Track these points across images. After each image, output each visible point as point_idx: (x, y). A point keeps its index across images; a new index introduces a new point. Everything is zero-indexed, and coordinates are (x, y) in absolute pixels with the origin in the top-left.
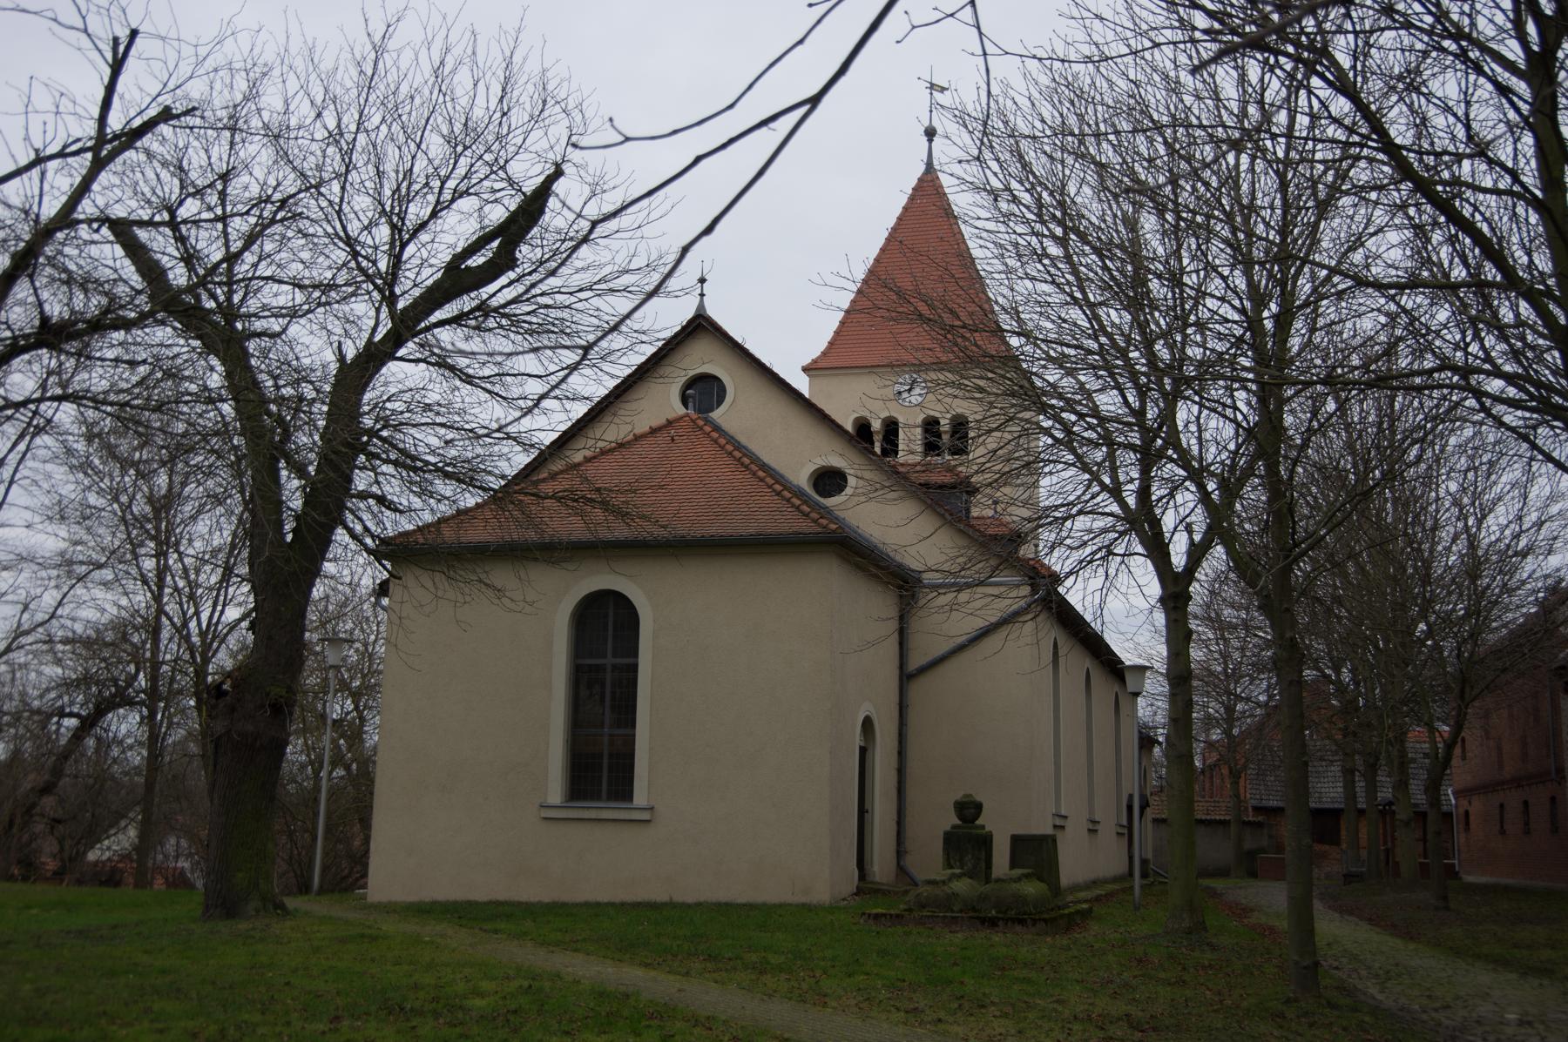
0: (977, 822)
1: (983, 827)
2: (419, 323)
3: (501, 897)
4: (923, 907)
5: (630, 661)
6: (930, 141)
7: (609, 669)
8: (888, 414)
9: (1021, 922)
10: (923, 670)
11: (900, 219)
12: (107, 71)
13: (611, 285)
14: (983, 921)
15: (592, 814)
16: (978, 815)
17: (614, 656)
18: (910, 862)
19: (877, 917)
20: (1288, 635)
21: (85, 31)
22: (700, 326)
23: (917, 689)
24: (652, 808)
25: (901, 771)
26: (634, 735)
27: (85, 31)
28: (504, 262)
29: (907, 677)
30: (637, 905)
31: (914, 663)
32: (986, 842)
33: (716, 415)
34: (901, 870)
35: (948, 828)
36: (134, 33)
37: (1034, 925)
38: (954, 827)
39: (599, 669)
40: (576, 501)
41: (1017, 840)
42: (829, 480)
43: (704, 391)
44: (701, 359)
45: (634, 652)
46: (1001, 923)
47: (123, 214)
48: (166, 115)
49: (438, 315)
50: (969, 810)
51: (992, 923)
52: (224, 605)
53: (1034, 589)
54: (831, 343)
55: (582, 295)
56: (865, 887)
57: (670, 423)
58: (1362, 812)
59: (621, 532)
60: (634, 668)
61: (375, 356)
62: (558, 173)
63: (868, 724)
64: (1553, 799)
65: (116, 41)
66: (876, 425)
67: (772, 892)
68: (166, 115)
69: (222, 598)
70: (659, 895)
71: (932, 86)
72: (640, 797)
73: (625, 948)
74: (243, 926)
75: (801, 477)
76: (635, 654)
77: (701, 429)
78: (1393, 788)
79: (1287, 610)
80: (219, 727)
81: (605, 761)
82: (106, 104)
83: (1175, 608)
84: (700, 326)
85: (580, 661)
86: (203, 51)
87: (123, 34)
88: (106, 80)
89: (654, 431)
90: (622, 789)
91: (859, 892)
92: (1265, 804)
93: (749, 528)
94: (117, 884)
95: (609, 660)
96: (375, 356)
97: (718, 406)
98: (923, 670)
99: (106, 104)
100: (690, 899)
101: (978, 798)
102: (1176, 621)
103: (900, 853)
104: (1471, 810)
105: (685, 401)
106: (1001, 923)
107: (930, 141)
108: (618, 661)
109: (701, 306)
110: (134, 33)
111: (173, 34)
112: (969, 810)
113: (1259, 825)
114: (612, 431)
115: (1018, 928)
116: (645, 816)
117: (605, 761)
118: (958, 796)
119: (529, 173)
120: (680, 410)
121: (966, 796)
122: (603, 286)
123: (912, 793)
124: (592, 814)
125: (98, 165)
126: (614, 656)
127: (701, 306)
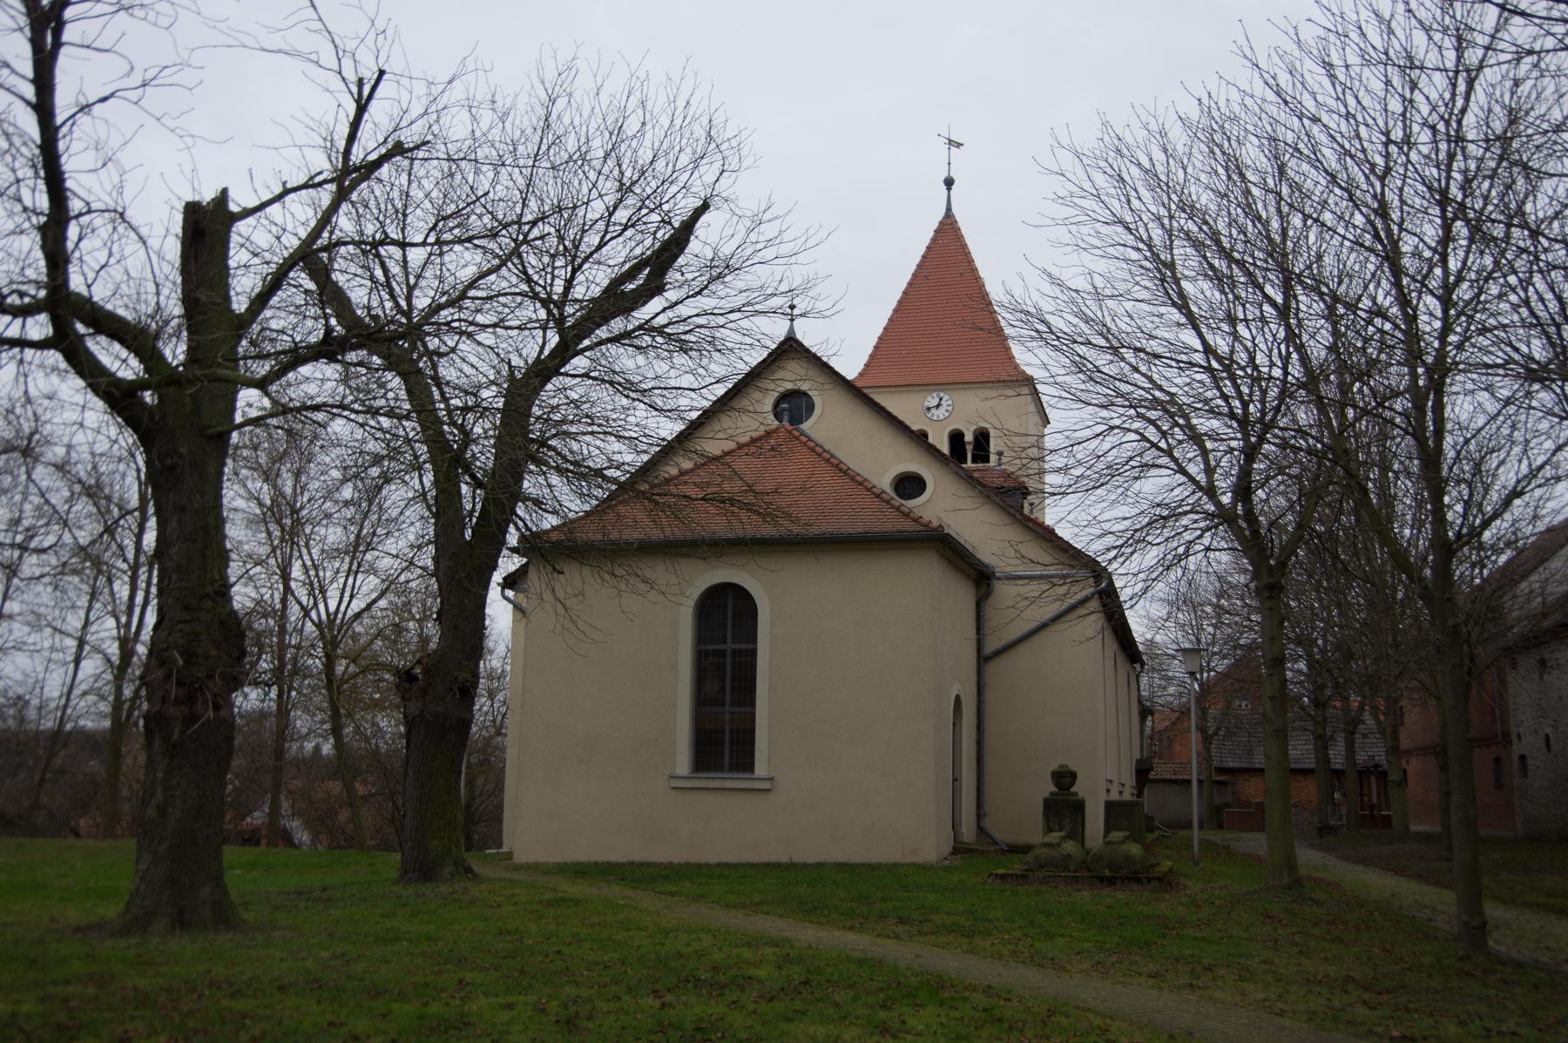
0: (1072, 790)
1: (1076, 794)
2: (581, 341)
3: (637, 858)
4: (1042, 867)
5: (749, 646)
6: (949, 189)
7: (729, 652)
8: (975, 427)
9: (1137, 880)
10: (999, 653)
11: (924, 257)
12: (352, 108)
13: (757, 307)
14: (1102, 879)
15: (718, 784)
16: (1073, 784)
17: (733, 642)
18: (988, 823)
19: (1003, 877)
20: (1451, 622)
21: (340, 73)
22: (790, 348)
23: (992, 669)
24: (771, 779)
25: (980, 743)
26: (754, 713)
27: (340, 73)
28: (655, 287)
29: (983, 660)
30: (767, 865)
31: (989, 648)
32: (1079, 807)
33: (805, 426)
34: (981, 830)
35: (1047, 795)
36: (382, 73)
37: (1149, 883)
38: (1052, 794)
39: (721, 654)
40: (724, 502)
41: (1110, 806)
42: (910, 485)
43: (794, 406)
44: (790, 377)
45: (753, 638)
46: (1118, 882)
47: (296, 243)
48: (399, 149)
49: (602, 333)
50: (1065, 778)
51: (1110, 881)
52: (352, 597)
53: (1097, 583)
54: (867, 365)
55: (732, 316)
56: (959, 849)
57: (768, 434)
58: (1339, 773)
59: (767, 530)
60: (753, 653)
61: (546, 369)
62: (704, 207)
63: (958, 699)
64: (1497, 760)
65: (360, 83)
66: (969, 437)
67: (884, 854)
68: (399, 149)
69: (348, 589)
70: (780, 855)
71: (950, 142)
72: (761, 768)
73: (811, 911)
74: (444, 889)
75: (885, 483)
76: (755, 640)
77: (797, 438)
78: (1387, 752)
79: (1449, 600)
80: (414, 708)
81: (727, 736)
82: (352, 138)
83: (1270, 597)
84: (790, 348)
85: (704, 647)
86: (435, 90)
87: (370, 75)
88: (351, 118)
89: (753, 441)
90: (743, 759)
91: (955, 851)
92: (1225, 765)
93: (858, 527)
94: (257, 843)
95: (729, 646)
96: (546, 369)
97: (807, 419)
98: (999, 653)
99: (352, 138)
100: (811, 860)
101: (1073, 767)
102: (1271, 609)
103: (980, 815)
104: (1409, 769)
105: (777, 416)
106: (1118, 882)
107: (949, 189)
108: (737, 646)
109: (791, 330)
110: (382, 73)
111: (406, 74)
112: (1065, 778)
113: (1225, 783)
114: (713, 444)
115: (1134, 886)
116: (766, 785)
117: (727, 736)
118: (1054, 766)
119: (684, 206)
120: (773, 422)
121: (1062, 766)
122: (750, 308)
123: (990, 763)
124: (718, 784)
125: (341, 196)
126: (733, 642)
127: (791, 330)
